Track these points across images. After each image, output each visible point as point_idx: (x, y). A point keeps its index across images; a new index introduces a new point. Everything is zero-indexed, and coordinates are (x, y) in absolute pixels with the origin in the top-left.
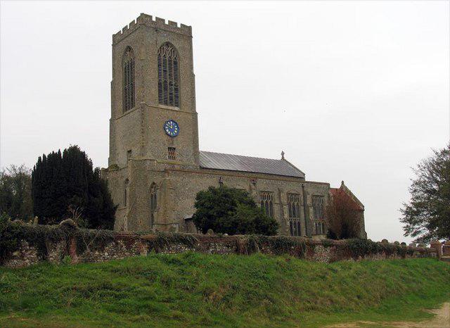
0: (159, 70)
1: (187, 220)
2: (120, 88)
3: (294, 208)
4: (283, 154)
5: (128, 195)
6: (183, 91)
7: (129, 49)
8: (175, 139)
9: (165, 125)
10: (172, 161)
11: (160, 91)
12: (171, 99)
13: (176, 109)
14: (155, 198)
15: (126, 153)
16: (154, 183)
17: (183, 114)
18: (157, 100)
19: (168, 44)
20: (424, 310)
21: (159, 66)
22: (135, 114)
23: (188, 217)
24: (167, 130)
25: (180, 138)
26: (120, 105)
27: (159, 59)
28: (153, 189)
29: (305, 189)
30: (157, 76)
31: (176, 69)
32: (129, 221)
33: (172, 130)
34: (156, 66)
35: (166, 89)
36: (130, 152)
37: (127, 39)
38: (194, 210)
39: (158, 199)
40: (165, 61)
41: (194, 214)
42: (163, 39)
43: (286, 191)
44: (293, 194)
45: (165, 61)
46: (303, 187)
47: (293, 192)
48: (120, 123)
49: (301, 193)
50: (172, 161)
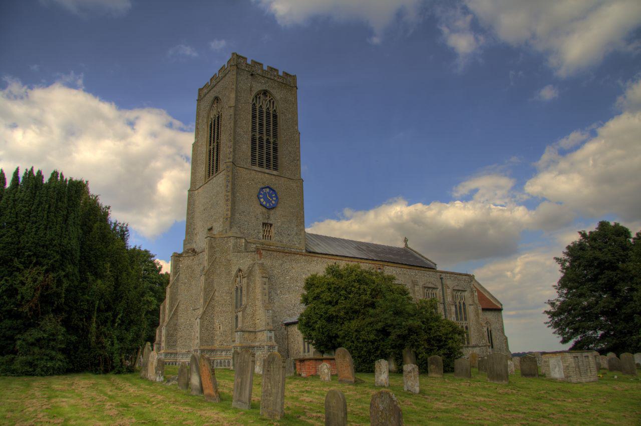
0: (254, 123)
1: (288, 324)
2: (203, 157)
3: (460, 307)
4: (406, 241)
5: (423, 259)
6: (283, 151)
7: (217, 99)
8: (272, 212)
9: (260, 193)
10: (267, 241)
11: (253, 149)
12: (268, 160)
13: (275, 173)
14: (241, 291)
15: (206, 230)
16: (240, 270)
17: (283, 179)
18: (244, 344)
19: (265, 93)
20: (377, 338)
21: (254, 117)
22: (220, 179)
23: (289, 320)
24: (262, 200)
25: (279, 211)
26: (202, 170)
27: (254, 109)
28: (238, 279)
29: (444, 281)
30: (250, 129)
31: (275, 124)
32: (202, 326)
33: (268, 201)
34: (250, 117)
35: (261, 147)
36: (210, 229)
37: (215, 89)
38: (302, 308)
39: (244, 292)
40: (261, 112)
41: (302, 315)
42: (258, 87)
43: (421, 284)
44: (429, 288)
45: (261, 112)
46: (441, 278)
47: (430, 285)
48: (201, 196)
49: (440, 287)
50: (267, 241)
